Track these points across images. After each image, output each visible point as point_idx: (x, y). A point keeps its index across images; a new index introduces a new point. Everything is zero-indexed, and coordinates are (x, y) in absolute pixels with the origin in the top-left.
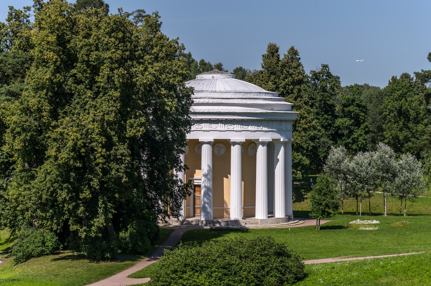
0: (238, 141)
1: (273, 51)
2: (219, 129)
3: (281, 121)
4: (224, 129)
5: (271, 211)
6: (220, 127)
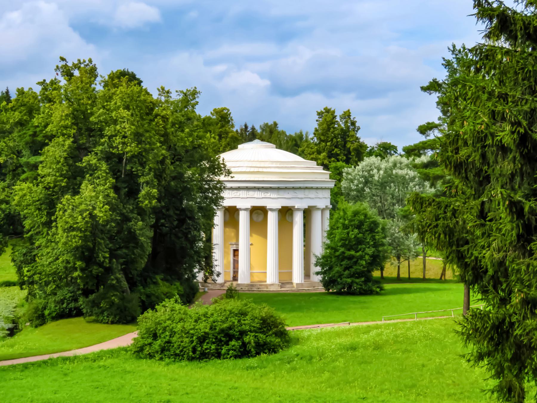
0: (274, 208)
2: (256, 196)
3: (317, 188)
4: (260, 196)
5: (307, 275)
6: (257, 194)
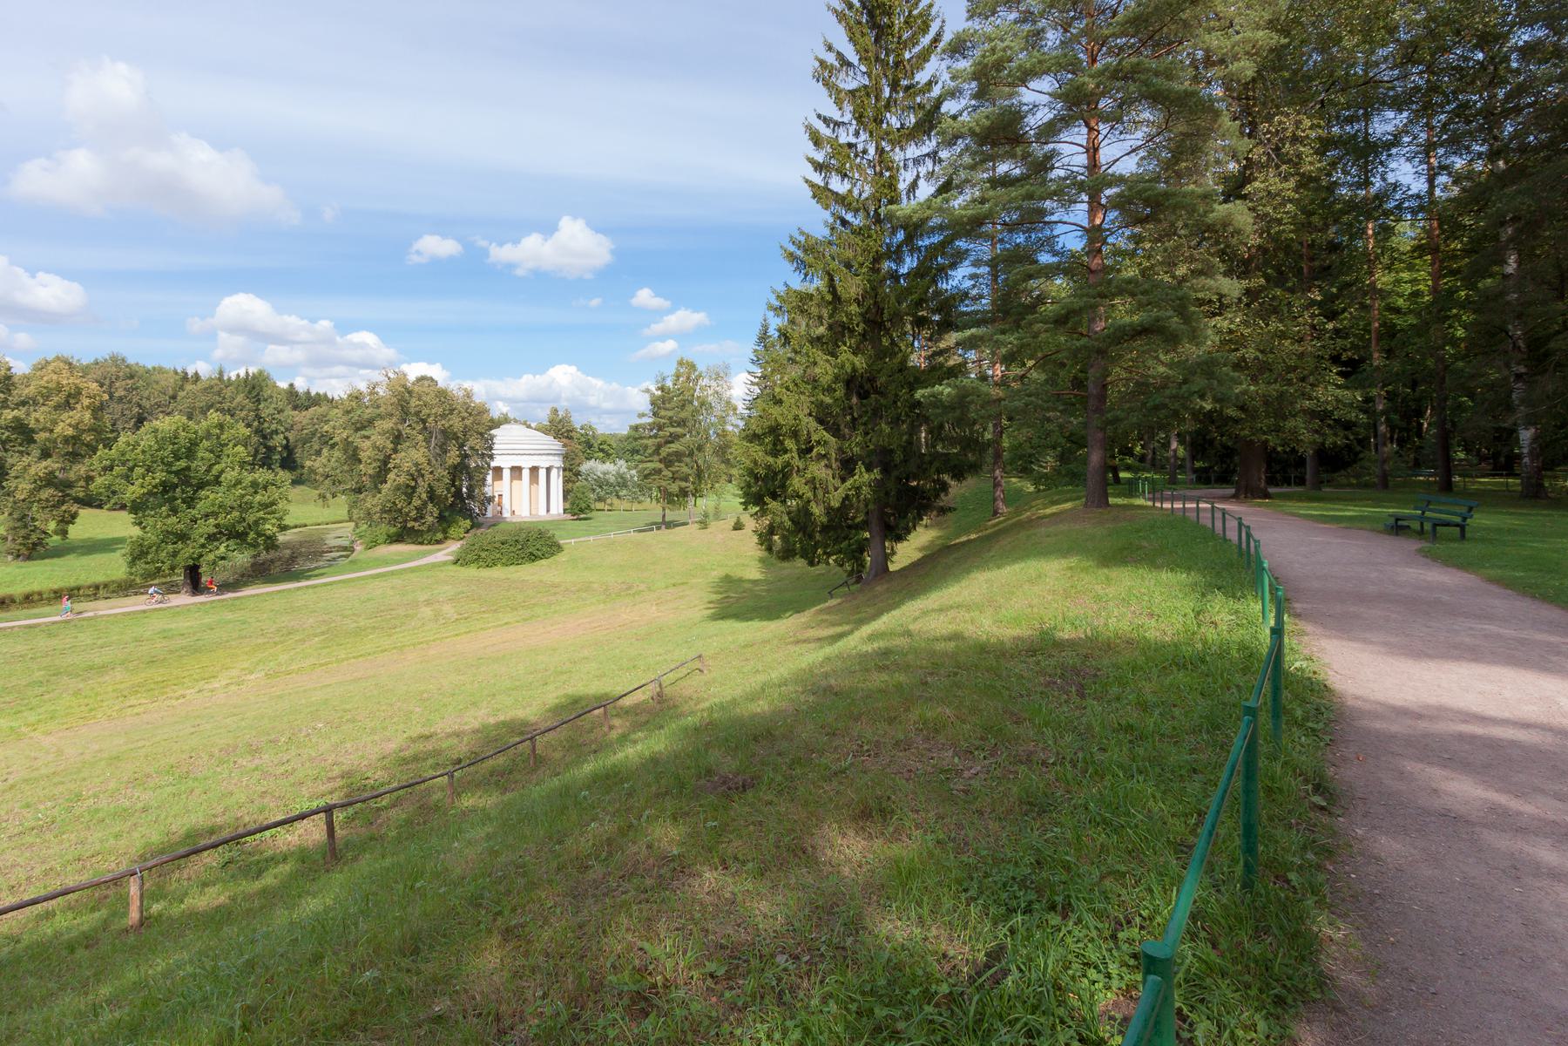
1: (555, 411)
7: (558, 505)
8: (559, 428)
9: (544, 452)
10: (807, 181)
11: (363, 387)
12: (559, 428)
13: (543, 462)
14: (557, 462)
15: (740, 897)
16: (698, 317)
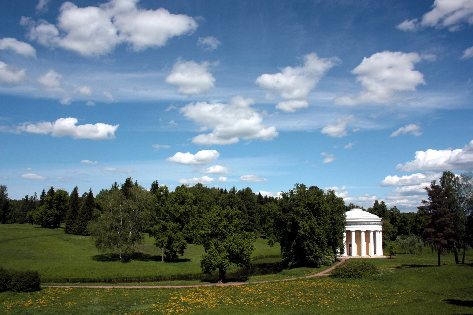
7: (380, 253)
8: (378, 209)
9: (374, 224)
10: (44, 190)
11: (287, 191)
12: (378, 209)
13: (372, 228)
14: (380, 228)
15: (168, 251)
16: (460, 150)
